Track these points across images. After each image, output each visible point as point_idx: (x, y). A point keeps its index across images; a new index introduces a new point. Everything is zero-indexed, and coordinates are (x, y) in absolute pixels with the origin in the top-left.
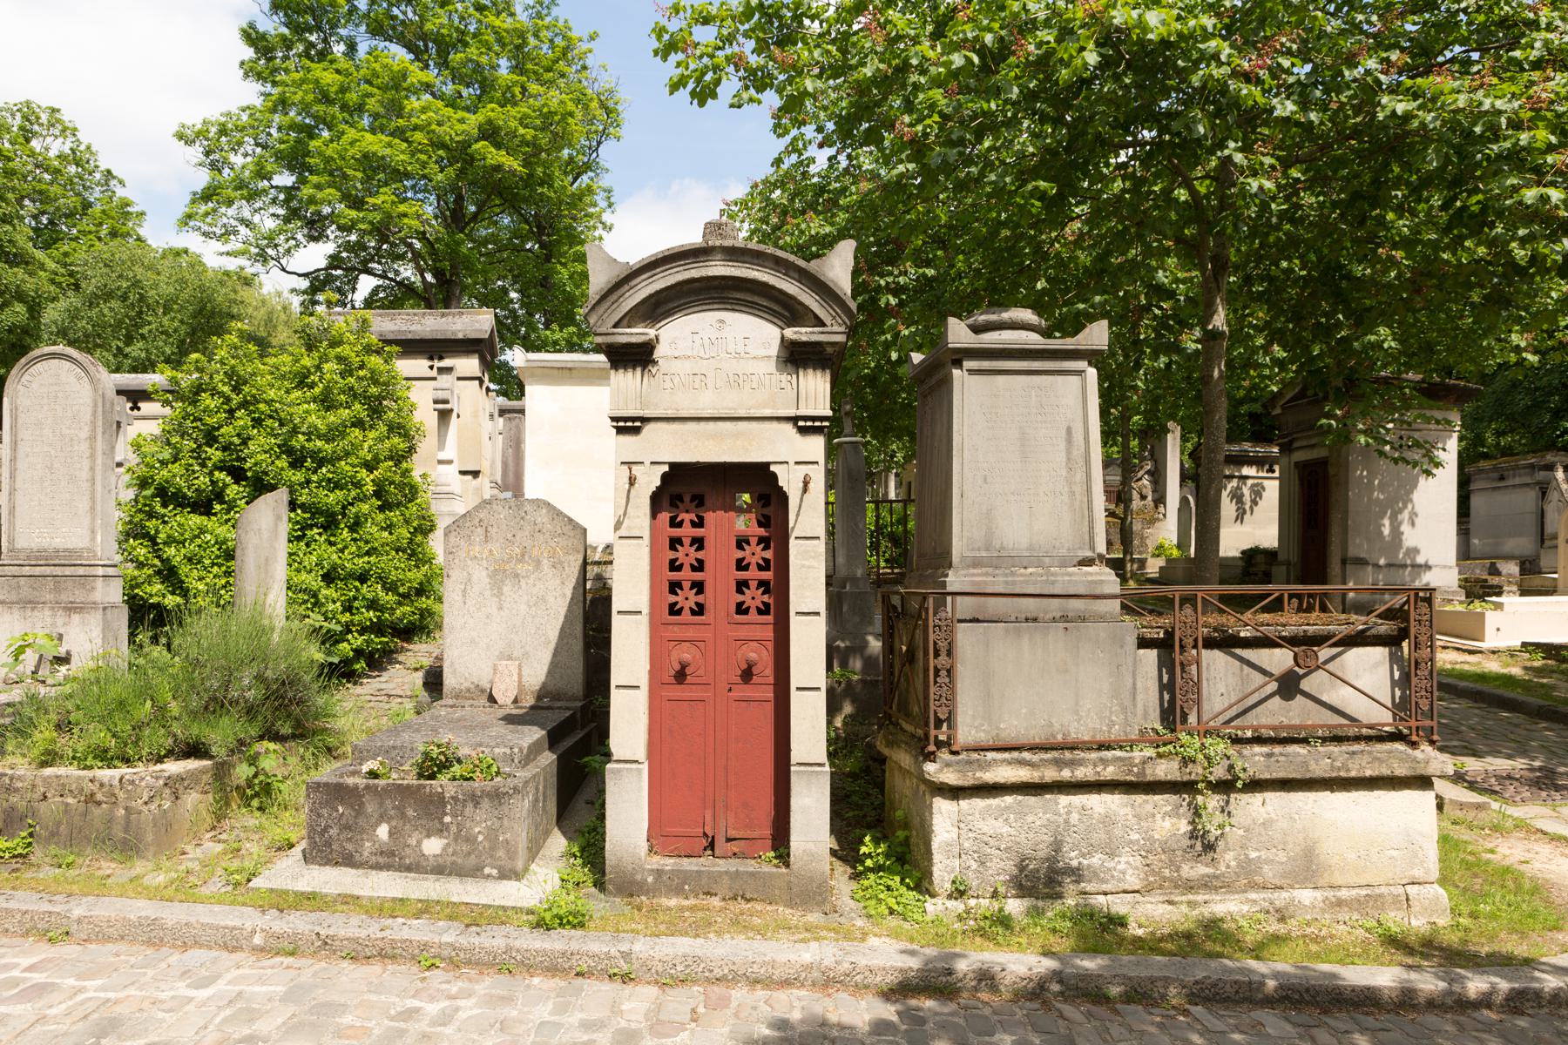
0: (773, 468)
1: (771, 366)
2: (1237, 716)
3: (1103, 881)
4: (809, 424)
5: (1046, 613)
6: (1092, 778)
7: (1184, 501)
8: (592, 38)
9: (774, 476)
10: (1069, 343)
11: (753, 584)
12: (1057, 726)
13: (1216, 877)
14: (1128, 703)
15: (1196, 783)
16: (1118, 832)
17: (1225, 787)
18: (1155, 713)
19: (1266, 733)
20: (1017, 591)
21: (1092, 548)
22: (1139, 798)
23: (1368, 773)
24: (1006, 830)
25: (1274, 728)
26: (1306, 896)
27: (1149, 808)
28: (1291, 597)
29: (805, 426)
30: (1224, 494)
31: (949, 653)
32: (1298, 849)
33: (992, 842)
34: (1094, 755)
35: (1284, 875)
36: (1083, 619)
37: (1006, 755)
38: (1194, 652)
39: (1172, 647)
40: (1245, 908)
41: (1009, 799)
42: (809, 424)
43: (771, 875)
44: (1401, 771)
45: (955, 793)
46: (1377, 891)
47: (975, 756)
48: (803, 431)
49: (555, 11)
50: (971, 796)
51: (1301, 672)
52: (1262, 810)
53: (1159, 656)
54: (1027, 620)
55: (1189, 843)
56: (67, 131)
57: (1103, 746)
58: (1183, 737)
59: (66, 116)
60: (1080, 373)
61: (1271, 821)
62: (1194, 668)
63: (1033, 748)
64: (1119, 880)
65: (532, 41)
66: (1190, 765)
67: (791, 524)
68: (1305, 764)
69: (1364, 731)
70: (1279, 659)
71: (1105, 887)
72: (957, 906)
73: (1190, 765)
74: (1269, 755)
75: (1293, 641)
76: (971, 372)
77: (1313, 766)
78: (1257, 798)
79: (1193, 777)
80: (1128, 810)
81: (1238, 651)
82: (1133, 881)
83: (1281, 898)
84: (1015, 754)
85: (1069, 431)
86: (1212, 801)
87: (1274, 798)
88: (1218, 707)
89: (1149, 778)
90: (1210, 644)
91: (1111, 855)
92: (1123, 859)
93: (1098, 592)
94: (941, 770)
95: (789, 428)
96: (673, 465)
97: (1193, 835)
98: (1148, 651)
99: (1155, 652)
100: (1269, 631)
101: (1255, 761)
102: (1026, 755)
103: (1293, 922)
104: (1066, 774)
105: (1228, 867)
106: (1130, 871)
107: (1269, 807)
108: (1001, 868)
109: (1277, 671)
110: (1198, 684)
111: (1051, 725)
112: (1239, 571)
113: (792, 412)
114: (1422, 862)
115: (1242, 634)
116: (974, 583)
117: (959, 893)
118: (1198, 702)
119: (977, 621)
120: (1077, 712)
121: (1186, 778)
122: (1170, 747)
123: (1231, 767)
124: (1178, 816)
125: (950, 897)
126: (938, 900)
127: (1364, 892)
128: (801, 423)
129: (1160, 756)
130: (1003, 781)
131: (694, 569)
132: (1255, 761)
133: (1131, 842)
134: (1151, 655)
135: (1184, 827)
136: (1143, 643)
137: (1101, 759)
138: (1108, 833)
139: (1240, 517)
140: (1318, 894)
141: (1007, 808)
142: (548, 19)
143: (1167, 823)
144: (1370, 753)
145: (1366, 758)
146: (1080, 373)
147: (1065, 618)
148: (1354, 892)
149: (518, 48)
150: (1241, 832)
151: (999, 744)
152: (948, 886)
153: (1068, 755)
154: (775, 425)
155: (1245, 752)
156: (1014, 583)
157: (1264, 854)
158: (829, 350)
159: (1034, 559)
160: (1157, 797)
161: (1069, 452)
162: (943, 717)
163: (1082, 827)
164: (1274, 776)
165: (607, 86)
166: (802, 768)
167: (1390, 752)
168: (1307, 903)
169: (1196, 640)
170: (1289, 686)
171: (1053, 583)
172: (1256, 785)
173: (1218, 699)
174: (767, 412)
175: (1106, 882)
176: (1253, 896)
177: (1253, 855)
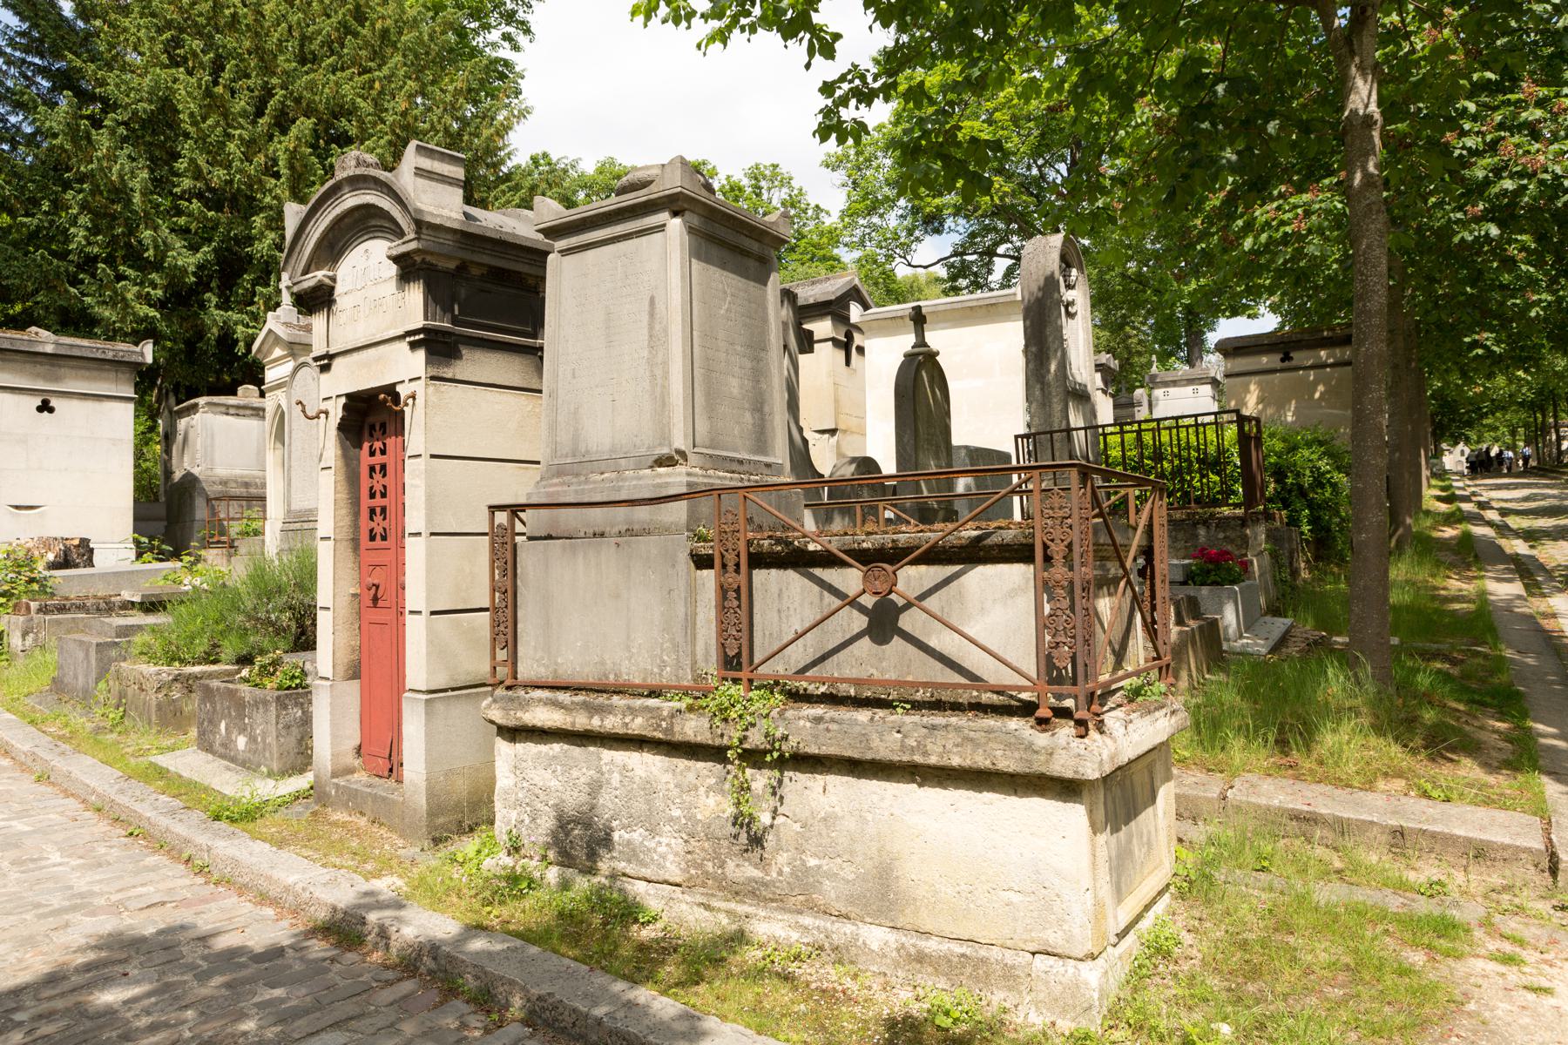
3: (643, 864)
12: (609, 665)
13: (765, 885)
16: (659, 804)
22: (682, 763)
23: (956, 761)
25: (857, 682)
26: (876, 936)
35: (851, 900)
36: (646, 532)
37: (545, 694)
40: (795, 936)
41: (557, 748)
44: (1008, 763)
46: (983, 952)
52: (822, 799)
55: (734, 831)
56: (786, 182)
57: (654, 693)
59: (784, 169)
69: (987, 697)
71: (645, 872)
74: (818, 720)
75: (865, 558)
77: (876, 742)
79: (725, 741)
80: (667, 777)
81: (818, 572)
82: (674, 872)
83: (843, 931)
86: (760, 780)
89: (678, 738)
92: (664, 840)
95: (403, 346)
96: (348, 396)
101: (803, 728)
104: (595, 723)
105: (780, 873)
106: (671, 857)
107: (832, 798)
111: (603, 663)
113: (400, 332)
114: (1060, 922)
115: (811, 547)
116: (549, 494)
119: (550, 537)
120: (628, 648)
121: (718, 742)
124: (722, 792)
127: (958, 949)
129: (690, 709)
130: (539, 724)
132: (803, 728)
135: (730, 810)
137: (629, 708)
138: (648, 802)
140: (892, 938)
144: (958, 729)
145: (953, 738)
148: (946, 946)
150: (797, 827)
153: (602, 699)
158: (418, 259)
159: (612, 462)
160: (700, 764)
167: (989, 731)
168: (875, 946)
170: (883, 622)
176: (807, 920)
177: (812, 862)
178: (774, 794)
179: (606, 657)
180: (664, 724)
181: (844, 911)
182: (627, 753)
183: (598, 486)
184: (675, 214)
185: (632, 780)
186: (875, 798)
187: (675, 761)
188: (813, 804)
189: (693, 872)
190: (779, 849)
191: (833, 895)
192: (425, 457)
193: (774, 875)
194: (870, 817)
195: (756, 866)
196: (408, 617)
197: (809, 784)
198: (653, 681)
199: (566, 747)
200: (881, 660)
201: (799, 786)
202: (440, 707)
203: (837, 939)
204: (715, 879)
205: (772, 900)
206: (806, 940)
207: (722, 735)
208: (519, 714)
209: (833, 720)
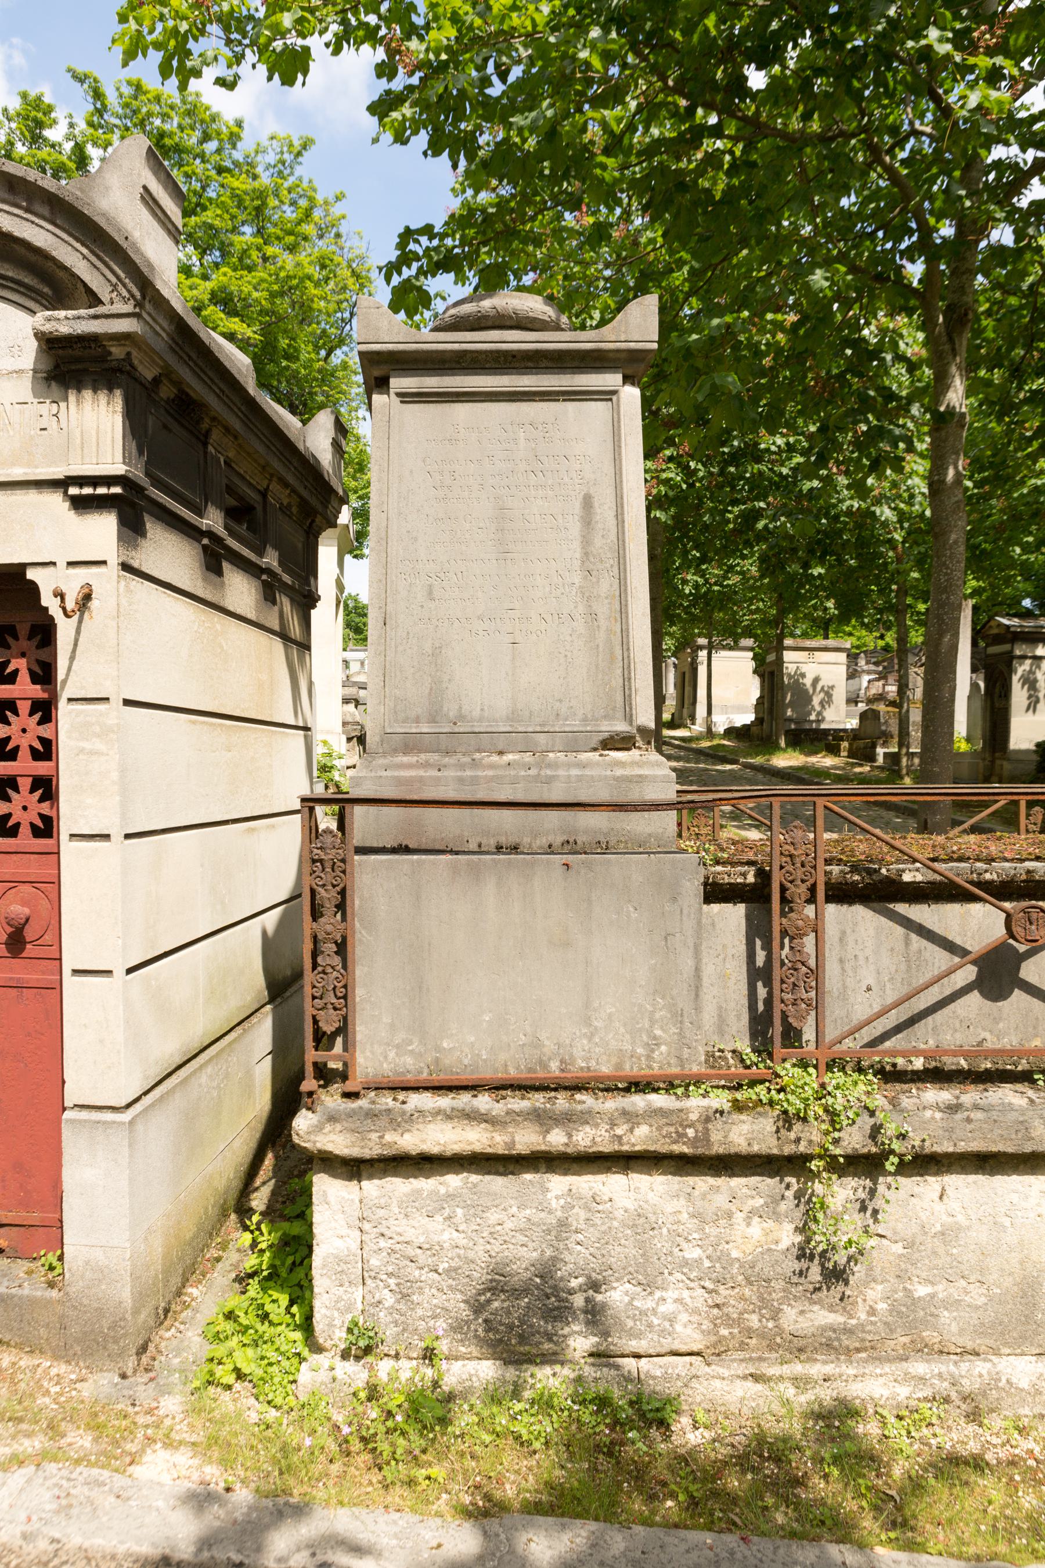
0: (31, 574)
1: (24, 388)
2: (898, 1029)
4: (87, 491)
5: (535, 836)
6: (607, 1148)
7: (974, 686)
8: (338, 199)
9: (33, 589)
10: (585, 341)
11: (25, 784)
12: (549, 1046)
13: (849, 1331)
14: (685, 1003)
15: (808, 1158)
16: (660, 1243)
17: (866, 1165)
18: (739, 1023)
19: (950, 1063)
20: (481, 796)
21: (629, 718)
22: (703, 1183)
24: (448, 1236)
27: (721, 1200)
28: (1030, 805)
29: (85, 495)
30: (1015, 678)
31: (341, 907)
32: (1008, 1282)
33: (422, 1258)
34: (612, 1104)
35: (981, 1330)
36: (604, 848)
37: (445, 1102)
38: (810, 911)
39: (767, 899)
41: (454, 1181)
42: (87, 491)
43: (33, 1302)
45: (354, 1168)
47: (387, 1100)
48: (80, 504)
49: (299, 171)
50: (384, 1173)
51: (1022, 948)
52: (938, 1207)
53: (748, 918)
54: (499, 849)
55: (797, 1266)
57: (637, 1086)
58: (789, 1072)
60: (608, 395)
61: (958, 1229)
62: (809, 941)
63: (500, 1087)
64: (662, 1333)
65: (272, 202)
66: (798, 1127)
67: (61, 675)
68: (1024, 1126)
70: (979, 924)
72: (355, 1373)
73: (798, 1127)
74: (953, 1109)
75: (1001, 891)
76: (406, 397)
78: (931, 1185)
79: (802, 1148)
80: (681, 1204)
81: (901, 908)
84: (464, 1099)
85: (588, 502)
86: (841, 1193)
87: (962, 1186)
88: (862, 1007)
90: (841, 894)
91: (649, 1286)
92: (671, 1294)
93: (635, 795)
94: (319, 1128)
95: (56, 501)
97: (804, 1253)
98: (727, 908)
99: (741, 909)
100: (955, 871)
102: (484, 1102)
103: (995, 1422)
104: (556, 1140)
105: (872, 1312)
106: (684, 1317)
107: (952, 1203)
108: (440, 1304)
109: (976, 945)
110: (817, 973)
111: (537, 1044)
112: (1033, 767)
113: (58, 472)
115: (907, 877)
116: (399, 782)
117: (362, 1348)
118: (818, 1007)
119: (406, 850)
120: (587, 1021)
121: (788, 1150)
122: (761, 1089)
123: (875, 1131)
124: (777, 1217)
125: (345, 1355)
126: (322, 1360)
128: (73, 491)
129: (738, 1107)
131: (36, 755)
132: (926, 1115)
133: (686, 1263)
134: (733, 916)
135: (787, 1237)
136: (716, 893)
137: (624, 1113)
138: (641, 1245)
139: (1033, 704)
141: (450, 1196)
142: (291, 179)
143: (756, 1230)
146: (608, 395)
147: (570, 846)
149: (259, 210)
150: (898, 1248)
151: (438, 1078)
152: (341, 1334)
153: (562, 1101)
154: (32, 496)
155: (906, 1102)
156: (474, 781)
157: (941, 1290)
158: (117, 352)
161: (586, 541)
162: (328, 1028)
163: (592, 1234)
164: (962, 1147)
165: (357, 252)
166: (84, 1115)
168: (1024, 1384)
169: (813, 889)
171: (549, 780)
172: (926, 1163)
173: (861, 997)
174: (18, 473)
175: (639, 1336)
176: (919, 1368)
177: (921, 1291)
178: (863, 1209)
179: (543, 1036)
180: (691, 1132)
181: (970, 1346)
182: (601, 1178)
183: (503, 774)
184: (627, 379)
185: (609, 1215)
186: (1015, 1198)
187: (691, 1180)
188: (923, 1216)
189: (724, 1332)
190: (871, 1279)
191: (954, 1328)
192: (116, 702)
193: (863, 1316)
194: (1007, 1222)
195: (831, 1309)
196: (70, 984)
197: (916, 1190)
198: (632, 1069)
199: (474, 1178)
200: (996, 1021)
201: (902, 1194)
202: (139, 1127)
203: (967, 1385)
204: (762, 1336)
205: (858, 1350)
206: (920, 1395)
207: (798, 1140)
208: (389, 1137)
209: (976, 1107)
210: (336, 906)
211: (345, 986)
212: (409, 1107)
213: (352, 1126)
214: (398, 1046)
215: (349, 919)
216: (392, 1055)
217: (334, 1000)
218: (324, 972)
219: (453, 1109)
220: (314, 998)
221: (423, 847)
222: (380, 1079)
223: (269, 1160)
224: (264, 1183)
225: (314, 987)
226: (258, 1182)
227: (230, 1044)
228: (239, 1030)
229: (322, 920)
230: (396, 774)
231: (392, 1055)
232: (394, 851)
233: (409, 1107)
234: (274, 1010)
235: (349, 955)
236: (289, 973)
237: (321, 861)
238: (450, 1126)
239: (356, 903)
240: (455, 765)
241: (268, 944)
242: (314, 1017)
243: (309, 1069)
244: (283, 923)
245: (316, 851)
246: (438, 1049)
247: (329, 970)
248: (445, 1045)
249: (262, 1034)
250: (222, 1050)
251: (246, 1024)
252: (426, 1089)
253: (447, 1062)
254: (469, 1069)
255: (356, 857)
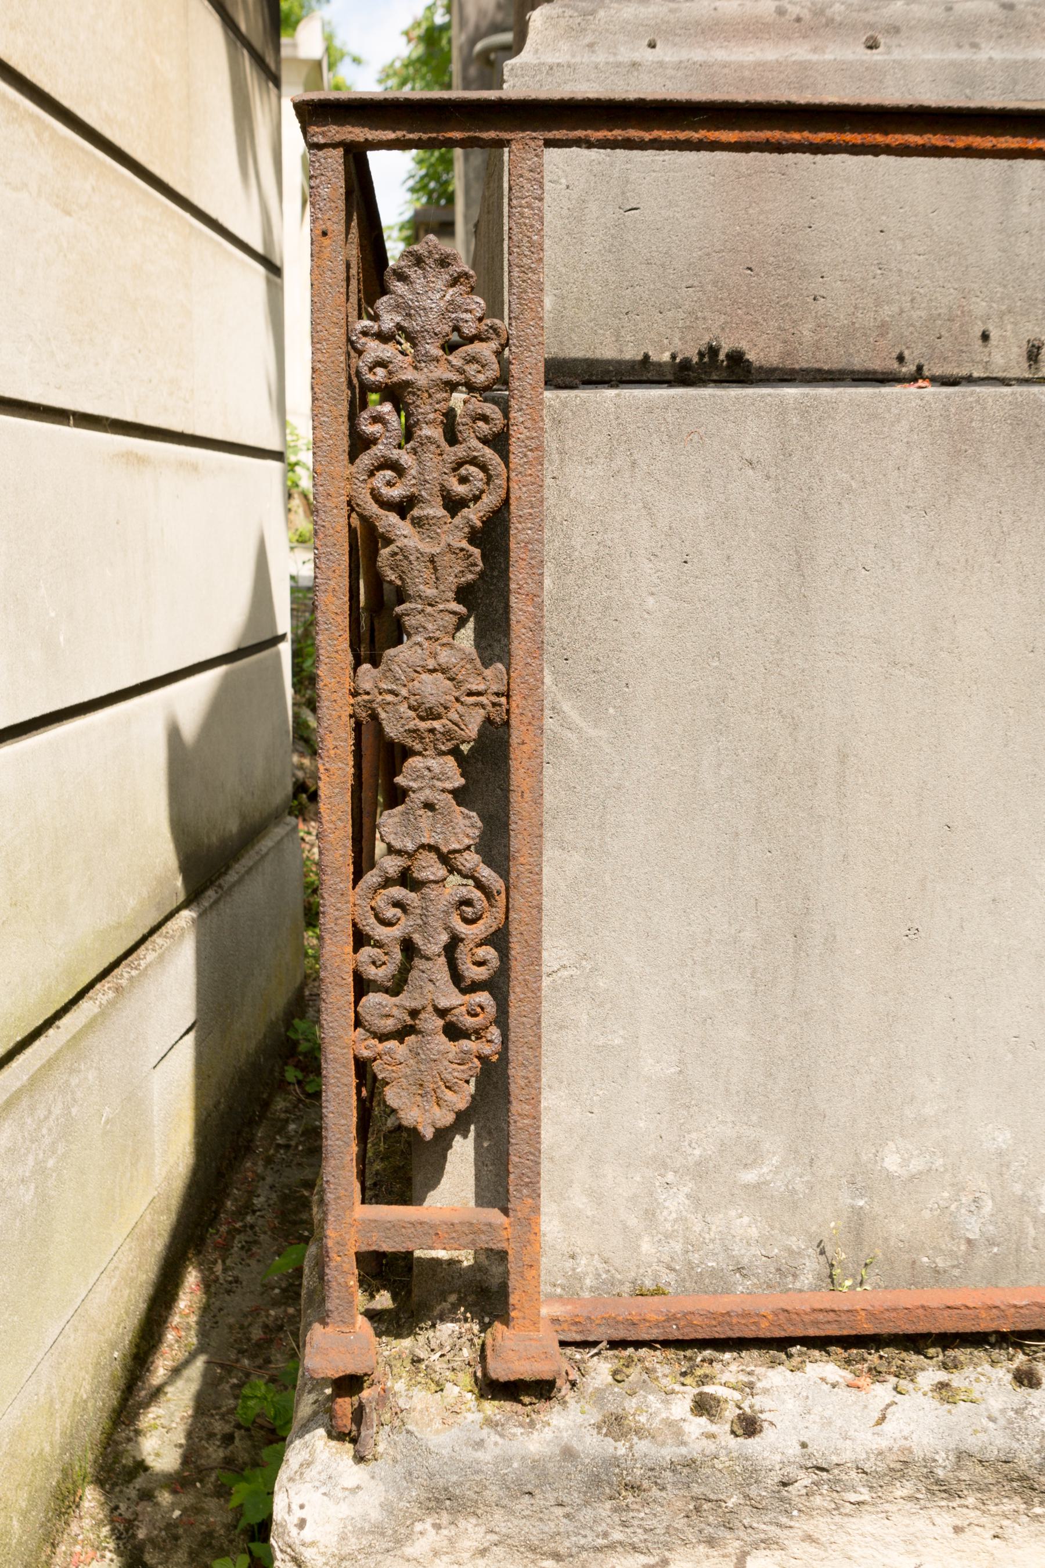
31: (487, 601)
47: (665, 1403)
119: (737, 370)
151: (866, 1300)
162: (423, 1116)
210: (463, 594)
211: (499, 939)
212: (773, 1447)
213: (534, 1531)
214: (700, 1171)
215: (520, 644)
216: (674, 1204)
217: (451, 998)
218: (406, 879)
219: (962, 1456)
220: (362, 986)
221: (804, 361)
222: (630, 1308)
223: (192, 1278)
224: (176, 1372)
225: (360, 939)
226: (160, 1370)
227: (75, 1039)
228: (103, 993)
229: (401, 655)
230: (698, 55)
231: (674, 1204)
232: (684, 374)
233: (773, 1447)
234: (199, 923)
235: (520, 805)
236: (233, 826)
237: (396, 394)
238: (946, 1520)
239: (550, 582)
240: (934, 27)
241: (183, 761)
242: (362, 1067)
243: (343, 1273)
244: (219, 708)
245: (375, 349)
246: (862, 1179)
247: (430, 868)
248: (892, 1162)
249: (171, 985)
250: (49, 1065)
251: (123, 972)
252: (821, 1343)
253: (898, 1229)
254: (982, 1259)
255: (548, 394)
